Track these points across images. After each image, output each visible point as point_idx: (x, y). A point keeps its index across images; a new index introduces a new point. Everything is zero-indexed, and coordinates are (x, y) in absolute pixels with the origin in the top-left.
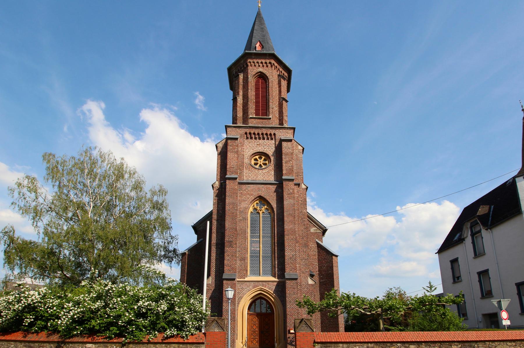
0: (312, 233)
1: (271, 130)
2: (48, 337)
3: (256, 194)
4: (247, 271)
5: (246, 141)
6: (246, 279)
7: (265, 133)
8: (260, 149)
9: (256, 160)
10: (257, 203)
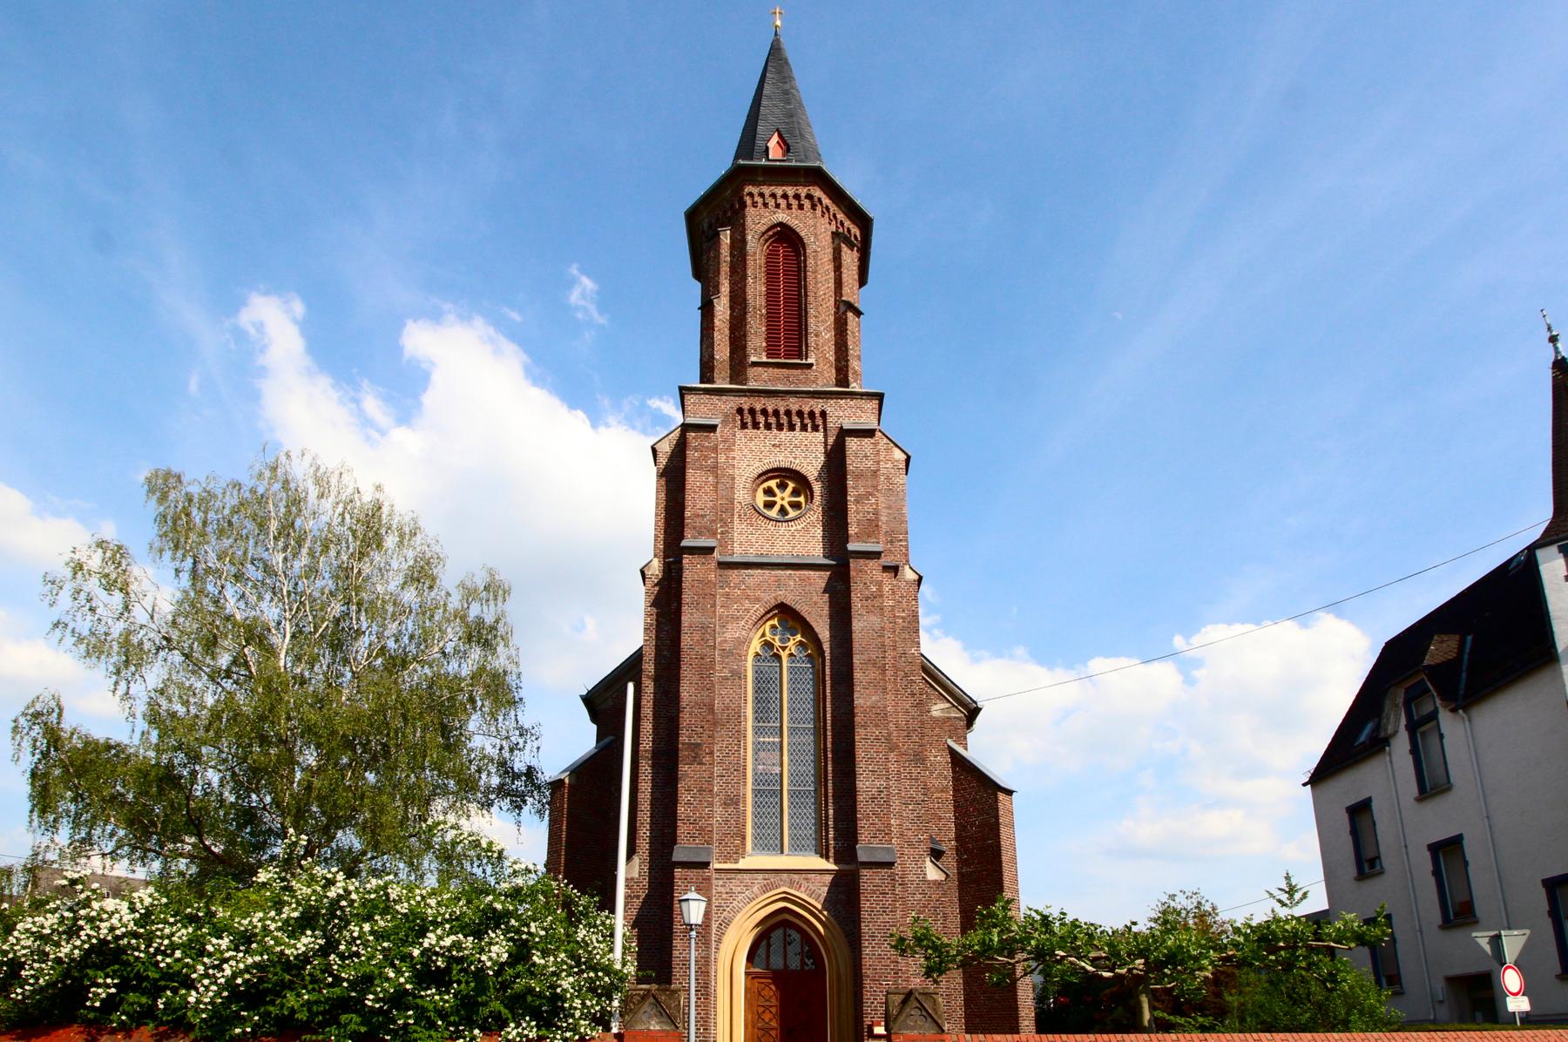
0: (936, 720)
3: (770, 598)
5: (740, 434)
6: (742, 864)
8: (781, 460)
9: (769, 492)
10: (773, 627)
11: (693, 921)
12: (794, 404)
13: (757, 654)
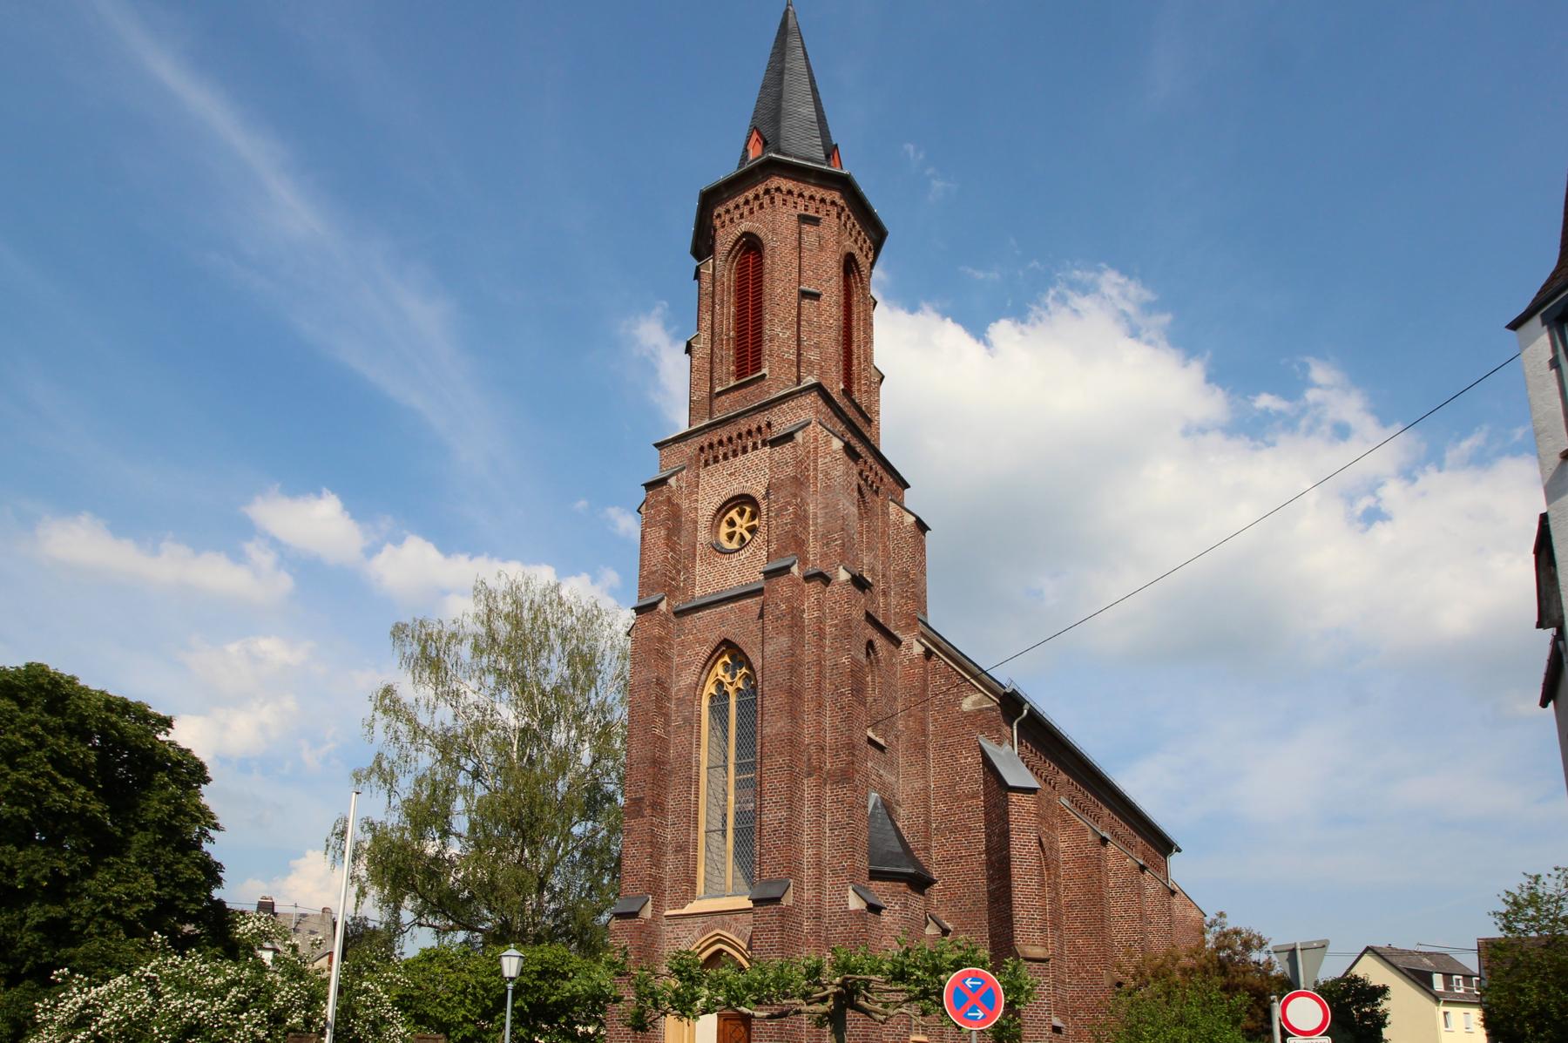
0: (967, 715)
1: (728, 428)
2: (1383, 991)
3: (714, 638)
4: (694, 883)
5: (702, 473)
6: (690, 908)
7: (744, 430)
8: (735, 488)
9: (732, 523)
10: (725, 664)
11: (506, 974)
12: (744, 425)
13: (712, 696)
